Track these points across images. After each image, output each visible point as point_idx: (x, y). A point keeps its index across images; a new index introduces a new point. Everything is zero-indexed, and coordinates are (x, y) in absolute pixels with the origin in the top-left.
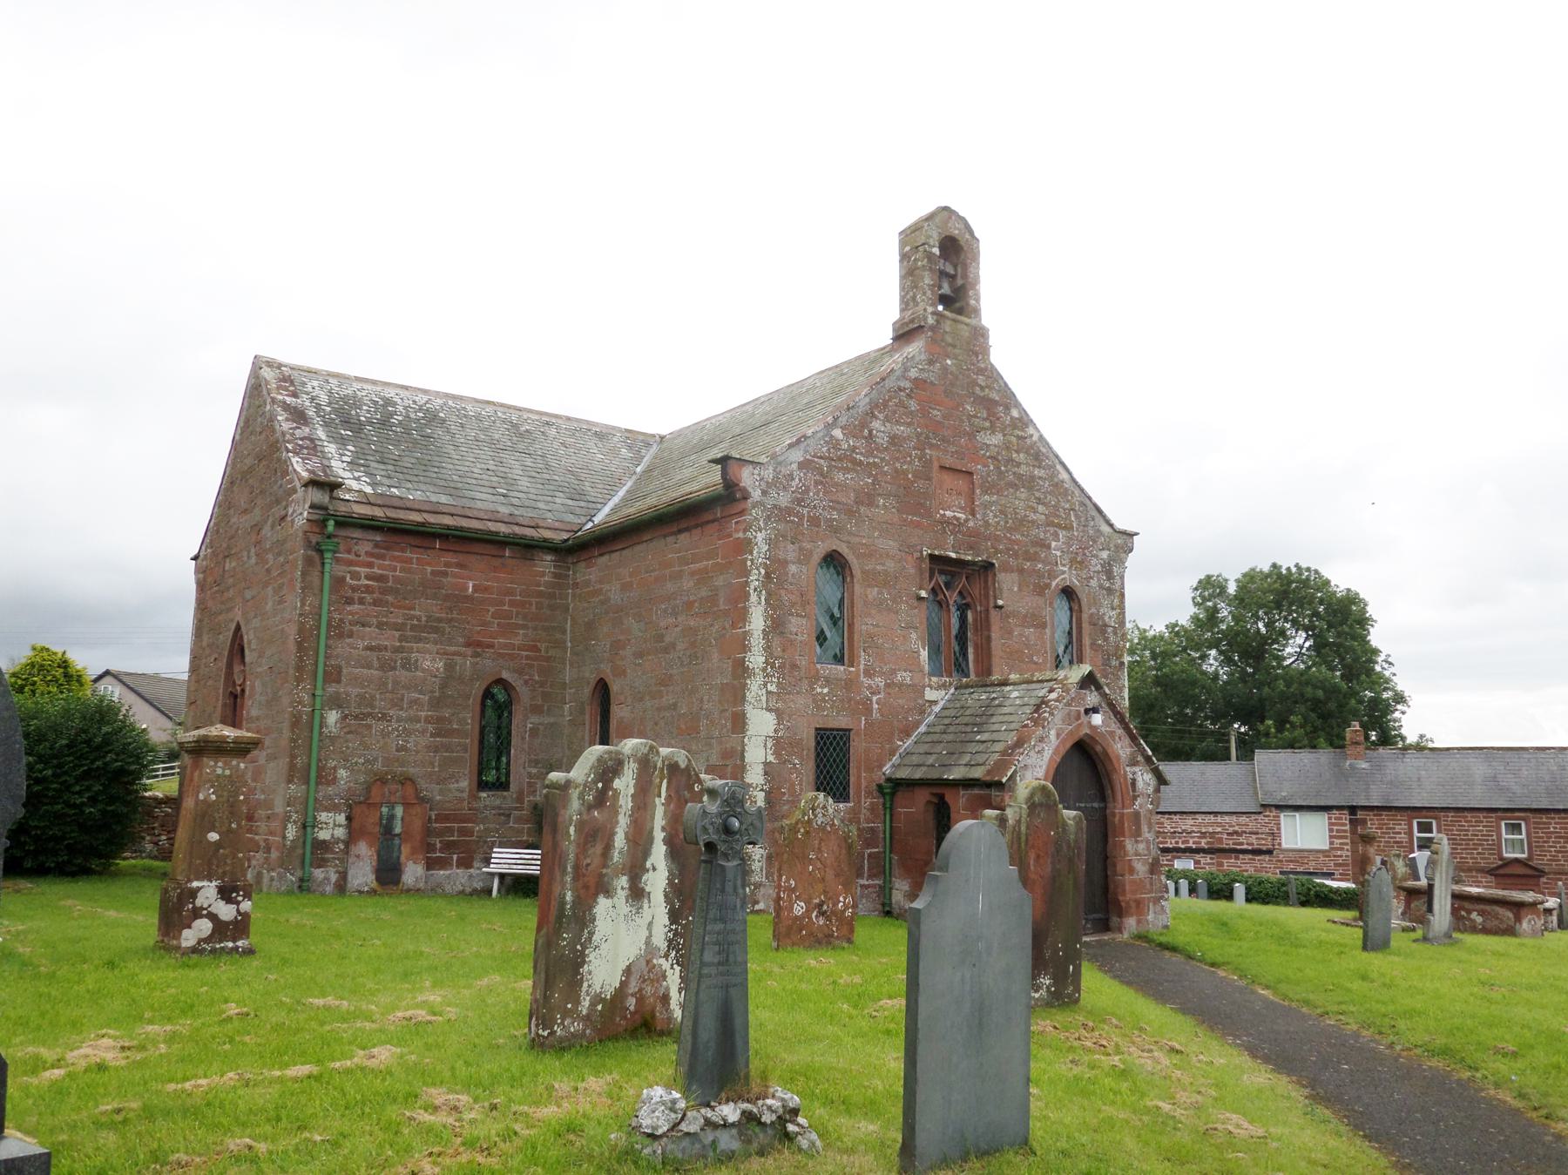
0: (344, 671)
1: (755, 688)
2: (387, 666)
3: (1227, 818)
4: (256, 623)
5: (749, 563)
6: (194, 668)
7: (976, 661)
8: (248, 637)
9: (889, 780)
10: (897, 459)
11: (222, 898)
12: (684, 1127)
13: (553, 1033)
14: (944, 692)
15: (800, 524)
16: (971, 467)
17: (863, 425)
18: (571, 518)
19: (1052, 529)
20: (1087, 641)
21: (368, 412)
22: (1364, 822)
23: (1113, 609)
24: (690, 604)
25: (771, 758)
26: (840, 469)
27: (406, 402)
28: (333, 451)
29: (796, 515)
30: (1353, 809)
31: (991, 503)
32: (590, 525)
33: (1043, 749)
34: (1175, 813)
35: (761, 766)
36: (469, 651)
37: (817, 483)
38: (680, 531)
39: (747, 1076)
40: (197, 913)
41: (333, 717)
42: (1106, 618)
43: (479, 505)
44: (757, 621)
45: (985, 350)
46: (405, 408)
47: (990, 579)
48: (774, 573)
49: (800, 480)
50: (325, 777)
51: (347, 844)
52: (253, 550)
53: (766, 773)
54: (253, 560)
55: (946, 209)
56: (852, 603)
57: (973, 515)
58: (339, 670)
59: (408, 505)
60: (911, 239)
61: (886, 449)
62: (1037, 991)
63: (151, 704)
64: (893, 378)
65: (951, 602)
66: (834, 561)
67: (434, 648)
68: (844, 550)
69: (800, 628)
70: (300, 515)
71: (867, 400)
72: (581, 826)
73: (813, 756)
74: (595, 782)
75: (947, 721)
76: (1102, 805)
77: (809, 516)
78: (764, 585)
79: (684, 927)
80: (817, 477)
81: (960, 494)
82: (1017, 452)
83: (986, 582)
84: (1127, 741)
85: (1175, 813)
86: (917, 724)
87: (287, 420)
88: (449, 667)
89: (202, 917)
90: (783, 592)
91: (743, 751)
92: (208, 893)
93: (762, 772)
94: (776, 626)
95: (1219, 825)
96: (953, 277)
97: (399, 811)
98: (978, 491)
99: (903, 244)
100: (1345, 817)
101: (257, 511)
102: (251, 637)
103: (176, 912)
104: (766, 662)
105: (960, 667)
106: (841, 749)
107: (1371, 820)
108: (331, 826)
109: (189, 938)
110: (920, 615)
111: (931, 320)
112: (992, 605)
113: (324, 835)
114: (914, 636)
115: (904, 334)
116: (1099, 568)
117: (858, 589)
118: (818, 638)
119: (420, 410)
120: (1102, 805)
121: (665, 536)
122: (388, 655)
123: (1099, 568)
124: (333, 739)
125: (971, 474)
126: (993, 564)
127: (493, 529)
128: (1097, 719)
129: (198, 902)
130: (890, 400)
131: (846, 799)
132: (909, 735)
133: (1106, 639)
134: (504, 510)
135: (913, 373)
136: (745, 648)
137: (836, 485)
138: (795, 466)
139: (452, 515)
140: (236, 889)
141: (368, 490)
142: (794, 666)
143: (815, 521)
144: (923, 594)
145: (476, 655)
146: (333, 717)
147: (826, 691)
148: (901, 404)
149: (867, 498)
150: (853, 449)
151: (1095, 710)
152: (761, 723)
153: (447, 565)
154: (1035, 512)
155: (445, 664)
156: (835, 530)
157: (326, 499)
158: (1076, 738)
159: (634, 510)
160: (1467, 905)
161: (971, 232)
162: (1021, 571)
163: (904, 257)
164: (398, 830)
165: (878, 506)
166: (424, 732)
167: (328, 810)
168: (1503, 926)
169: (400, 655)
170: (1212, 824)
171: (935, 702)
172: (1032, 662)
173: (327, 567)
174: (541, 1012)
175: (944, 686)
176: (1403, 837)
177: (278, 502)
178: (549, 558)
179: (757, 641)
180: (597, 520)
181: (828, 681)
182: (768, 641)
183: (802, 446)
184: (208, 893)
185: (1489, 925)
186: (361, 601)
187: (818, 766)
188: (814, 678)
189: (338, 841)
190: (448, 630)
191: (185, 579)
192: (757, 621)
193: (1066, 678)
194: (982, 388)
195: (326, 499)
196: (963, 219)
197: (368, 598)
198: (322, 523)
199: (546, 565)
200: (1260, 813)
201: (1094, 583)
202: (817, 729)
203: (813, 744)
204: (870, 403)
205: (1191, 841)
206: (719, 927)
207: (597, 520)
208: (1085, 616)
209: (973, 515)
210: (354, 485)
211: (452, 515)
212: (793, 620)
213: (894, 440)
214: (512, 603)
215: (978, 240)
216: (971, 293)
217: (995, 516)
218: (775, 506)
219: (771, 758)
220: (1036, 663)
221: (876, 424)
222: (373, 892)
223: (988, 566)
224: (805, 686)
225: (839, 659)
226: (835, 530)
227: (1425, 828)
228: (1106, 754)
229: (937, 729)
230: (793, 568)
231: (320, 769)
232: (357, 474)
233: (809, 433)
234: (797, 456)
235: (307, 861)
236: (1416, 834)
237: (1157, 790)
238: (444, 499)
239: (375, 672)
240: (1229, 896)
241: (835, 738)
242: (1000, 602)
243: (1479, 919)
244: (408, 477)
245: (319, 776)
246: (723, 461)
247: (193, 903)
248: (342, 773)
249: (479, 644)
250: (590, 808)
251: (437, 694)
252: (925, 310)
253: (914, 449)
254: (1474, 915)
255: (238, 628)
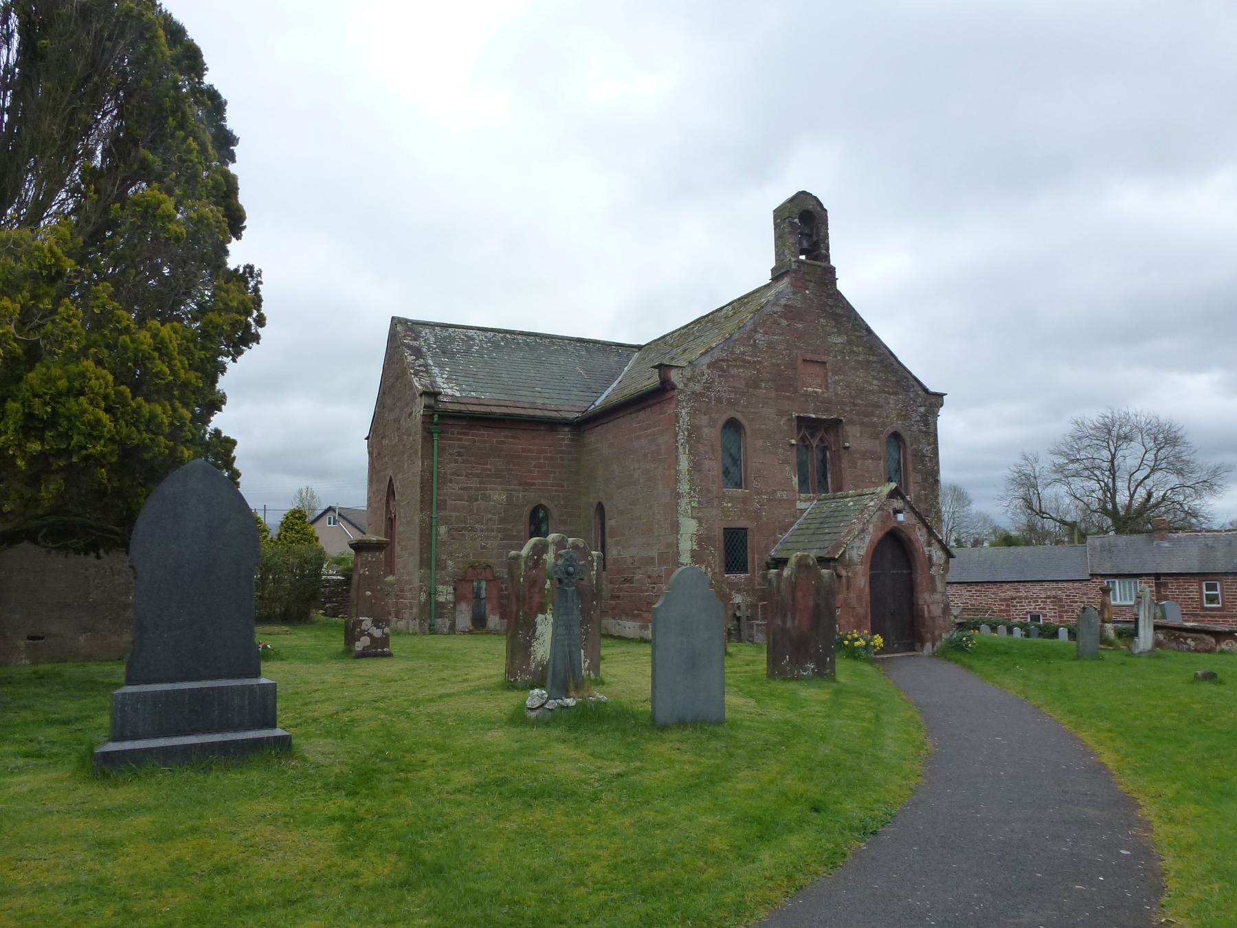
0: (448, 503)
1: (684, 503)
2: (471, 499)
3: (1065, 585)
4: (400, 476)
5: (677, 429)
6: (369, 505)
7: (833, 482)
8: (397, 485)
9: (773, 559)
10: (773, 357)
11: (375, 626)
12: (547, 706)
13: (516, 680)
14: (809, 503)
15: (710, 402)
16: (824, 358)
17: (750, 337)
18: (578, 404)
19: (883, 395)
20: (910, 467)
21: (458, 345)
22: (1165, 585)
23: (929, 445)
24: (645, 455)
25: (695, 547)
26: (734, 366)
27: (481, 338)
28: (437, 372)
29: (707, 397)
30: (1157, 576)
31: (839, 381)
32: (593, 406)
33: (864, 537)
34: (1028, 582)
35: (689, 552)
36: (521, 487)
37: (719, 376)
38: (640, 410)
39: (820, 801)
40: (362, 633)
41: (443, 530)
42: (924, 451)
43: (524, 399)
44: (684, 464)
45: (833, 281)
46: (480, 341)
47: (840, 431)
48: (694, 431)
49: (709, 375)
50: (441, 566)
51: (454, 604)
52: (396, 434)
53: (692, 557)
54: (397, 440)
55: (804, 192)
56: (746, 448)
57: (827, 388)
58: (445, 502)
59: (481, 402)
60: (781, 215)
61: (765, 352)
62: (805, 671)
63: (356, 527)
64: (769, 306)
65: (814, 446)
66: (733, 425)
67: (500, 487)
68: (739, 417)
69: (713, 466)
70: (419, 410)
71: (752, 321)
72: (526, 577)
73: (722, 546)
74: (533, 555)
75: (809, 521)
76: (909, 572)
77: (715, 397)
78: (688, 442)
79: (585, 630)
80: (720, 373)
81: (818, 376)
82: (857, 346)
83: (838, 432)
84: (924, 530)
85: (1028, 582)
86: (792, 524)
87: (410, 355)
88: (509, 498)
89: (365, 635)
90: (700, 446)
91: (678, 543)
92: (367, 623)
93: (689, 556)
94: (696, 467)
95: (1060, 589)
96: (810, 236)
97: (484, 584)
98: (830, 374)
99: (775, 218)
100: (1152, 581)
101: (397, 410)
102: (398, 484)
103: (351, 635)
104: (691, 489)
105: (823, 486)
106: (741, 541)
107: (1172, 583)
108: (445, 594)
109: (359, 646)
110: (793, 456)
111: (794, 266)
112: (841, 446)
113: (441, 599)
114: (788, 468)
115: (777, 275)
116: (918, 418)
117: (749, 440)
118: (724, 473)
119: (489, 341)
120: (909, 572)
121: (631, 413)
122: (473, 492)
123: (918, 418)
124: (444, 543)
125: (824, 363)
126: (842, 421)
127: (531, 414)
128: (901, 517)
129: (363, 627)
130: (766, 320)
131: (746, 571)
132: (786, 531)
133: (924, 465)
134: (540, 401)
135: (783, 301)
136: (677, 481)
137: (732, 376)
138: (705, 367)
139: (507, 407)
140: (381, 621)
141: (458, 394)
142: (709, 491)
143: (719, 400)
144: (793, 442)
145: (525, 490)
146: (443, 530)
147: (730, 505)
148: (775, 322)
149: (754, 384)
150: (743, 353)
151: (900, 512)
152: (689, 526)
153: (506, 437)
154: (871, 384)
155: (507, 497)
156: (732, 404)
157: (432, 402)
158: (887, 529)
159: (618, 398)
160: (1185, 634)
161: (821, 205)
162: (862, 424)
163: (776, 226)
164: (483, 595)
165: (761, 388)
166: (495, 538)
167: (443, 584)
168: (1208, 647)
169: (480, 492)
170: (1054, 589)
171: (804, 510)
172: (870, 481)
173: (435, 443)
174: (511, 671)
175: (810, 500)
176: (1195, 595)
177: (407, 405)
178: (566, 429)
179: (684, 477)
180: (597, 403)
181: (731, 499)
182: (691, 476)
183: (709, 354)
184: (367, 623)
185: (1200, 647)
186: (456, 462)
187: (726, 551)
188: (722, 498)
189: (450, 602)
190: (507, 476)
191: (359, 453)
192: (684, 464)
193: (881, 492)
194: (831, 307)
195: (432, 402)
196: (816, 197)
197: (460, 459)
198: (432, 416)
199: (565, 435)
200: (1089, 580)
201: (915, 428)
202: (724, 529)
203: (722, 538)
204: (753, 323)
205: (1040, 601)
206: (565, 617)
207: (597, 403)
208: (909, 451)
209: (827, 389)
210: (449, 392)
211: (507, 407)
212: (706, 462)
213: (771, 345)
214: (546, 458)
215: (826, 211)
216: (822, 245)
217: (842, 389)
218: (693, 393)
219: (695, 547)
220: (874, 483)
221: (758, 336)
222: (470, 632)
223: (838, 422)
224: (716, 503)
225: (738, 485)
226: (732, 404)
227: (1211, 587)
228: (910, 539)
229: (804, 526)
230: (706, 430)
231: (438, 560)
232: (451, 385)
233: (714, 345)
234: (707, 360)
235: (433, 614)
236: (1205, 592)
237: (947, 562)
238: (506, 397)
239: (466, 503)
240: (1054, 634)
241: (737, 534)
242: (847, 444)
243: (1193, 644)
244: (481, 384)
245: (437, 565)
246: (659, 367)
247: (360, 628)
248: (450, 563)
249: (527, 484)
250: (531, 569)
251: (503, 515)
252: (790, 260)
253: (785, 349)
254: (1189, 641)
255: (391, 480)
